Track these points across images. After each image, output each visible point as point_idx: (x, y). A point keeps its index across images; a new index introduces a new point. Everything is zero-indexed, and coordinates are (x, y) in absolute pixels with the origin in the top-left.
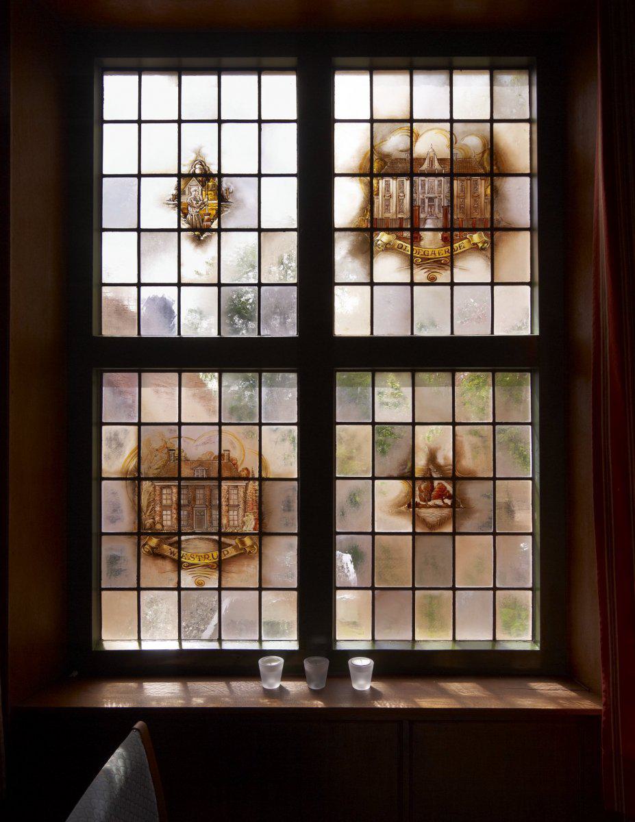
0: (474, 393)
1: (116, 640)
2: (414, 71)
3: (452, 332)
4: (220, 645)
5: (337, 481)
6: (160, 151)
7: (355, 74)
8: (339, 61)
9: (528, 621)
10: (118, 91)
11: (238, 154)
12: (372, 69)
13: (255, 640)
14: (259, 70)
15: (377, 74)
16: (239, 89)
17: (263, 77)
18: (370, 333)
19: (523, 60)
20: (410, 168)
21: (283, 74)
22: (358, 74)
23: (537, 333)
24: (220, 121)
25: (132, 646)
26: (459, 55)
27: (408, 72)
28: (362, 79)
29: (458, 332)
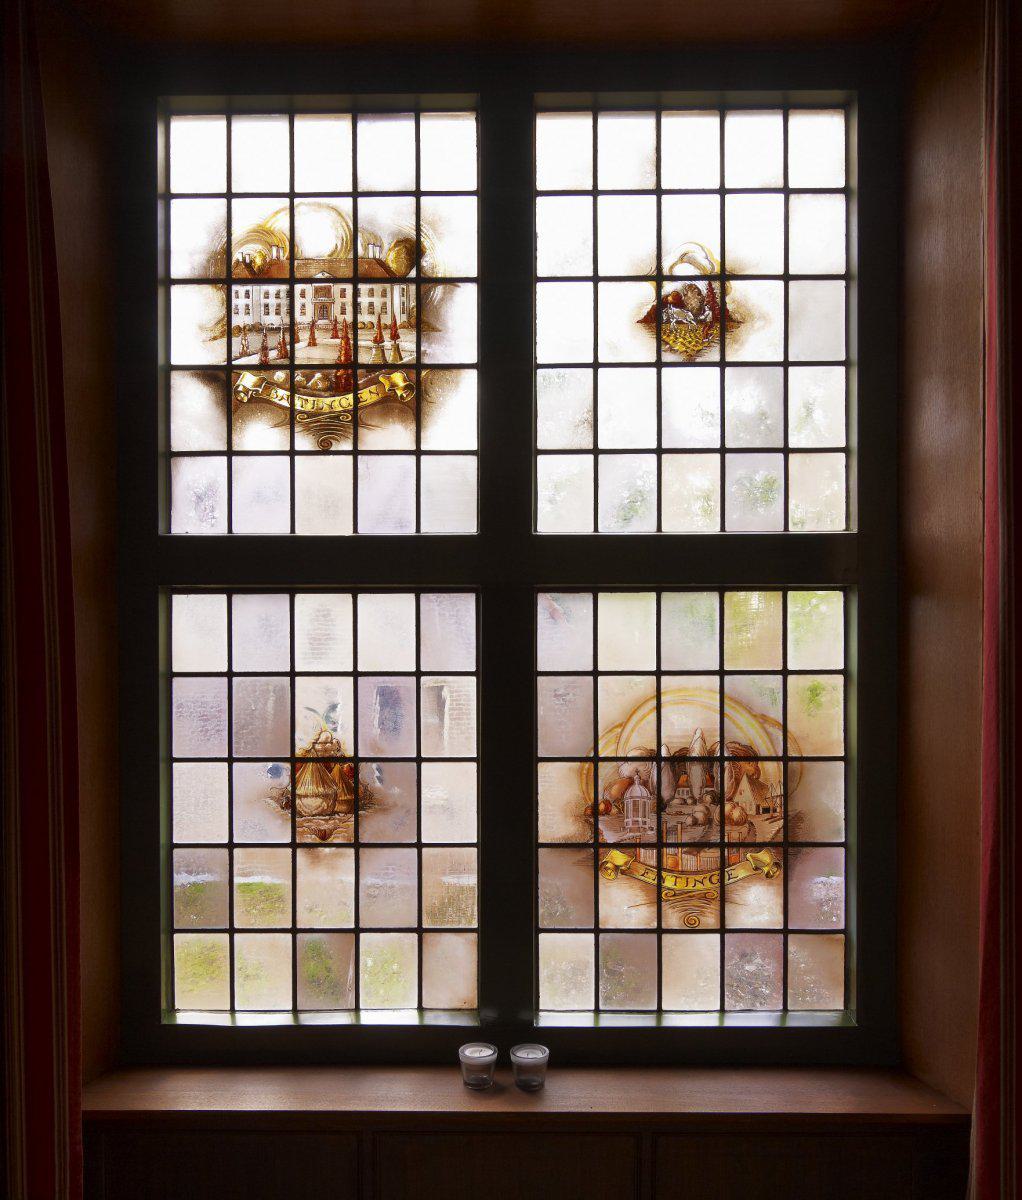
0: (386, 623)
1: (195, 1006)
2: (359, 115)
3: (596, 529)
4: (233, 1018)
5: (540, 764)
6: (628, 234)
7: (699, 115)
8: (541, 98)
9: (578, 1004)
10: (193, 147)
11: (754, 237)
12: (229, 112)
13: (589, 1011)
14: (786, 108)
15: (667, 116)
16: (754, 137)
17: (665, 121)
18: (844, 527)
19: (838, 95)
20: (284, 271)
21: (396, 118)
22: (683, 115)
23: (854, 530)
24: (723, 191)
25: (343, 1019)
26: (423, 93)
27: (653, 114)
28: (579, 125)
29: (241, 528)
